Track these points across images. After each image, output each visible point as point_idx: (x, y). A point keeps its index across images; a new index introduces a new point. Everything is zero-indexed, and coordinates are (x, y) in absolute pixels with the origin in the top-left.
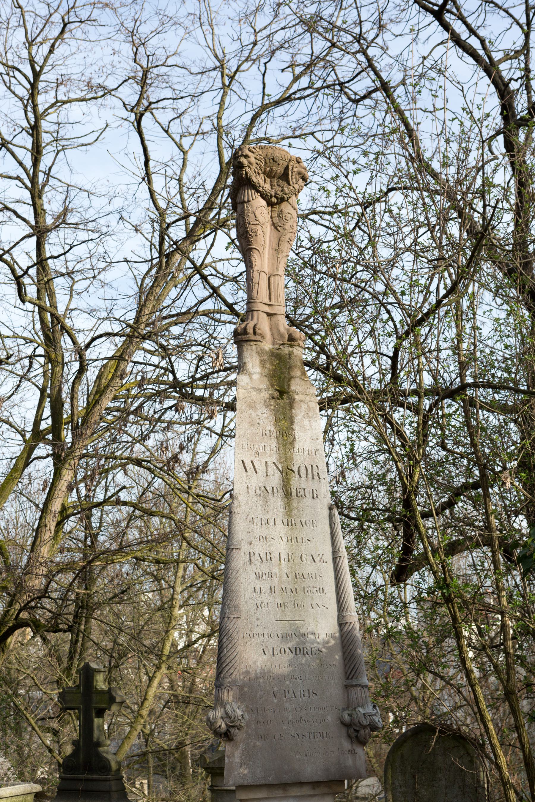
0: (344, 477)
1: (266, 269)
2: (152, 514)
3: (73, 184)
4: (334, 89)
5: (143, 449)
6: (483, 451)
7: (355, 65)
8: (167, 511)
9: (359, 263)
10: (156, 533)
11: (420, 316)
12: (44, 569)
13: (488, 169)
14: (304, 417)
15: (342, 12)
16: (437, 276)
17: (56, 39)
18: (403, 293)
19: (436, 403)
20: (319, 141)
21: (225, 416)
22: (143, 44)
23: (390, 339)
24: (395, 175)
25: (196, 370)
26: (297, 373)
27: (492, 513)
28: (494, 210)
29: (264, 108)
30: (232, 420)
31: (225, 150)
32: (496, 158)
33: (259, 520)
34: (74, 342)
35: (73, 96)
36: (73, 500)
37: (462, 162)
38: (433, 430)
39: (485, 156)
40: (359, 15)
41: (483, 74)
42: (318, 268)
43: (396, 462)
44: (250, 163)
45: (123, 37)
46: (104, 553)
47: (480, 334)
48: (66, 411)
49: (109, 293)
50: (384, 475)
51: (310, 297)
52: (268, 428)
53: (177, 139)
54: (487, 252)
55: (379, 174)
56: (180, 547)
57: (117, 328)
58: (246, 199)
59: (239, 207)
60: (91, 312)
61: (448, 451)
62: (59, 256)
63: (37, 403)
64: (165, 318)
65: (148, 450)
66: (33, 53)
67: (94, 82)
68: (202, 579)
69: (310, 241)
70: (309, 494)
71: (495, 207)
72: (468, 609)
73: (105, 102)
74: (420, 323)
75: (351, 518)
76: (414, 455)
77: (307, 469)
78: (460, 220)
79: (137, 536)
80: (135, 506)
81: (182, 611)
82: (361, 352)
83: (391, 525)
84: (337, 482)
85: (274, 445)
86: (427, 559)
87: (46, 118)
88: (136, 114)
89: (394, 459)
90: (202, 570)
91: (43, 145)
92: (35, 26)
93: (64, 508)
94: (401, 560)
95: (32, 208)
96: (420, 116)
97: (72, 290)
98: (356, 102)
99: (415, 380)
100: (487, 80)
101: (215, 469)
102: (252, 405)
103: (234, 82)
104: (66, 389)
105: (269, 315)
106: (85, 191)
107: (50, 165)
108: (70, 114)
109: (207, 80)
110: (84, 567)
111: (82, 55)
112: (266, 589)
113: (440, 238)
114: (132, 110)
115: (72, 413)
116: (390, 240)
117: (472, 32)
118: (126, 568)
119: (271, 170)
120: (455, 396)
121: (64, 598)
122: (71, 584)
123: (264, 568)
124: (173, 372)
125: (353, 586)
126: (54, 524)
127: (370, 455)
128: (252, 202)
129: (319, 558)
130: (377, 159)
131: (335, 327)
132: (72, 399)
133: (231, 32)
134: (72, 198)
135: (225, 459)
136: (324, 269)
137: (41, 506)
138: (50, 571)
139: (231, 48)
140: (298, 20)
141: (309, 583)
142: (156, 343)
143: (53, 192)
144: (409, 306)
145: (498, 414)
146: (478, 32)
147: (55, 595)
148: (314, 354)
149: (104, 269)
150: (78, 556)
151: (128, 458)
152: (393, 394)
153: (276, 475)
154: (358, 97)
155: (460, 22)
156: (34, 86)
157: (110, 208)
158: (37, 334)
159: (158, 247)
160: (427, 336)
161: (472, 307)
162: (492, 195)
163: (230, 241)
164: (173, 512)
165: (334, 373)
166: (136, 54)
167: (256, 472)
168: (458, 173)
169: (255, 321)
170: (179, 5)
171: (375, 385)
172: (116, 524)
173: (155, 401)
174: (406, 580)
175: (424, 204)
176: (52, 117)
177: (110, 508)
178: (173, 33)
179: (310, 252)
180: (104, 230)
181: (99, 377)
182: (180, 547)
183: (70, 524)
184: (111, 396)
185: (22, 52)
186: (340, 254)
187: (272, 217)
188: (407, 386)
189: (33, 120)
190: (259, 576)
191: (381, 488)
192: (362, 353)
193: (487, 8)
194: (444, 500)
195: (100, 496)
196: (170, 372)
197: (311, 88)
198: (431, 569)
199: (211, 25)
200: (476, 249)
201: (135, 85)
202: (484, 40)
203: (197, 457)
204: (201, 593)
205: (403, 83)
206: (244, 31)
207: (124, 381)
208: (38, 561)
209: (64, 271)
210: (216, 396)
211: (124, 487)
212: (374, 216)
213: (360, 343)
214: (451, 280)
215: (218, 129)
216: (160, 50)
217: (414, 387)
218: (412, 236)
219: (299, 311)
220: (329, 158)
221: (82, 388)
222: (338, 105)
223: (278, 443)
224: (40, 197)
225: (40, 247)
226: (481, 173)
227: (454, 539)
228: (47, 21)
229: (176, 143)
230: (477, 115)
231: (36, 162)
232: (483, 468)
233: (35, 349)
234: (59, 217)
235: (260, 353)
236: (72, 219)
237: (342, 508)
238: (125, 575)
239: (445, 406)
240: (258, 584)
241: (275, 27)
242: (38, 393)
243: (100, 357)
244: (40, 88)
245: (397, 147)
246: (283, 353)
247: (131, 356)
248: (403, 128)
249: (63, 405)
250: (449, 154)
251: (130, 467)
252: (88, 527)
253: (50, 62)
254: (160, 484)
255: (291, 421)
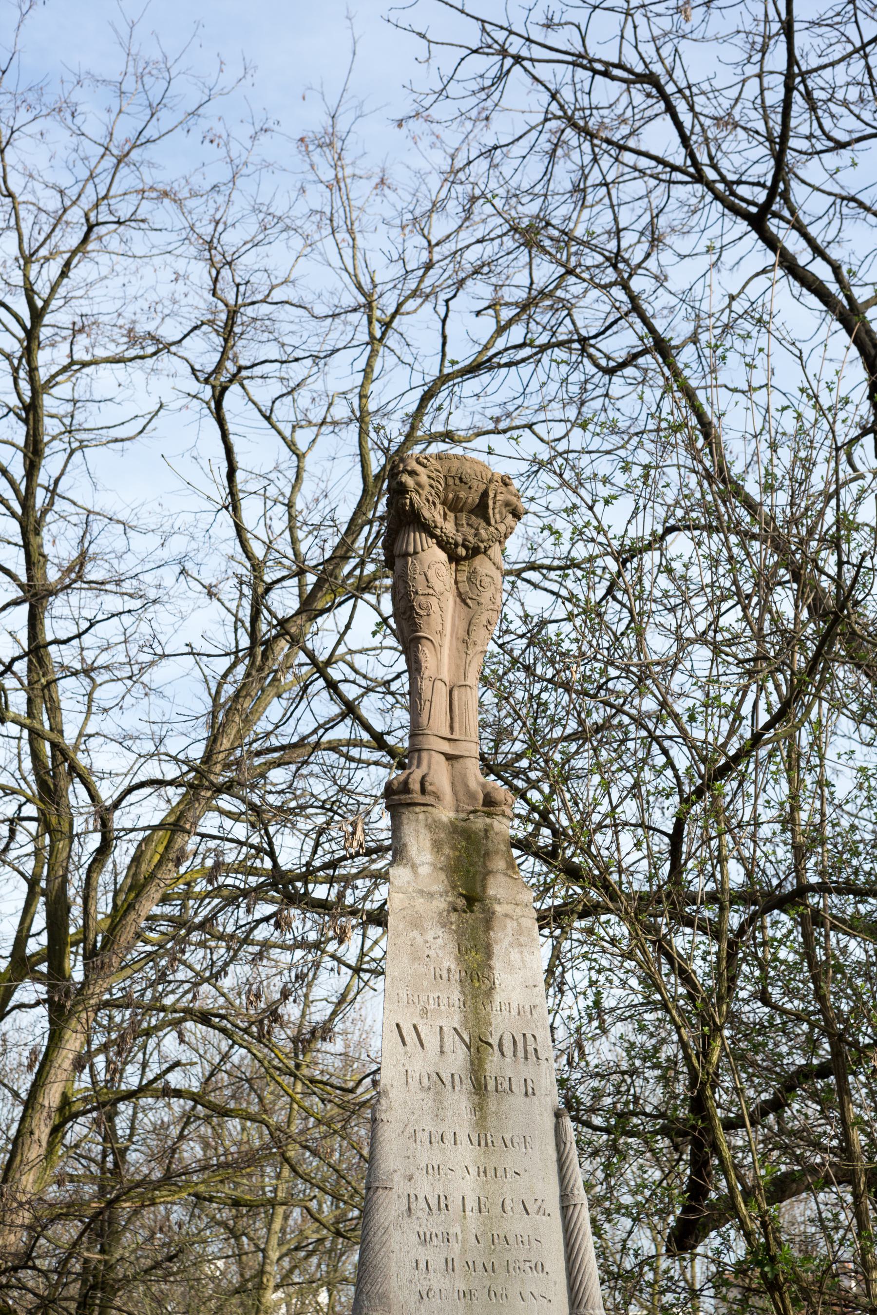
0: (582, 1055)
1: (445, 675)
2: (226, 1113)
3: (97, 510)
4: (570, 349)
5: (213, 991)
6: (838, 1008)
7: (607, 308)
8: (254, 1109)
9: (612, 664)
10: (233, 1149)
11: (723, 761)
12: (26, 1214)
13: (847, 496)
14: (511, 945)
15: (586, 213)
16: (754, 687)
17: (74, 253)
18: (692, 719)
19: (751, 920)
20: (542, 440)
21: (364, 936)
22: (229, 264)
23: (667, 803)
24: (677, 502)
25: (315, 852)
26: (499, 864)
27: (854, 1124)
28: (858, 572)
29: (443, 379)
30: (376, 943)
31: (372, 453)
32: (862, 477)
33: (427, 1134)
34: (94, 796)
35: (100, 353)
36: (83, 1085)
37: (799, 484)
38: (745, 968)
39: (841, 475)
40: (616, 219)
41: (837, 325)
42: (539, 670)
43: (678, 1028)
44: (419, 484)
45: (193, 251)
46: (138, 1184)
47: (832, 793)
48: (75, 920)
49: (157, 708)
50: (656, 1049)
51: (524, 724)
52: (446, 964)
53: (287, 433)
54: (845, 645)
55: (650, 504)
56: (278, 1177)
57: (172, 771)
58: (411, 550)
59: (398, 563)
60: (124, 740)
61: (775, 1007)
62: (70, 639)
63: (22, 904)
64: (258, 754)
65: (223, 995)
66: (32, 276)
67: (142, 328)
68: (315, 1237)
69: (525, 623)
70: (518, 1088)
71: (860, 566)
72: (811, 1304)
73: (160, 365)
74: (722, 772)
75: (596, 1128)
76: (712, 1016)
77: (515, 1042)
78: (795, 586)
79: (199, 1153)
80: (196, 1098)
81: (280, 1294)
82: (616, 825)
83: (667, 1141)
84: (569, 1063)
85: (456, 995)
86: (734, 1208)
87: (52, 391)
88: (213, 387)
89: (673, 1021)
90: (317, 1220)
91: (46, 439)
92: (37, 227)
93: (65, 1101)
94: (686, 1210)
95: (22, 553)
96: (724, 399)
97: (90, 700)
98: (610, 372)
99: (713, 875)
100: (844, 338)
101: (345, 1033)
102: (416, 923)
103: (390, 332)
104: (76, 881)
105: (450, 758)
106: (118, 522)
107: (57, 474)
108: (95, 385)
109: (341, 327)
110: (100, 1213)
111: (121, 280)
112: (438, 1263)
113: (761, 619)
114: (206, 381)
115: (86, 926)
116: (669, 620)
117: (818, 251)
118: (178, 1213)
119: (457, 498)
120: (786, 906)
121: (62, 1269)
122: (75, 1244)
123: (434, 1225)
124: (272, 855)
125: (598, 1257)
126: (47, 1131)
127: (631, 1014)
128: (422, 555)
129: (536, 1207)
130: (646, 476)
131: (567, 779)
132: (86, 900)
133: (387, 246)
134: (95, 534)
135: (363, 1012)
136: (550, 673)
137: (24, 1096)
138: (37, 1219)
139: (386, 273)
140: (506, 227)
141: (518, 1253)
142: (243, 800)
143: (62, 524)
144: (704, 742)
145: (864, 940)
146: (828, 251)
147: (43, 1264)
148: (530, 828)
149: (152, 664)
150: (90, 1189)
151: (186, 1010)
152: (673, 903)
153: (459, 1052)
154: (612, 364)
155: (795, 234)
156: (31, 335)
157: (164, 554)
158: (24, 779)
159: (248, 625)
160: (735, 795)
161: (817, 745)
162: (853, 545)
163: (379, 620)
164: (265, 1111)
165: (567, 862)
166: (215, 281)
167: (422, 1045)
168: (792, 504)
169: (424, 768)
170: (294, 195)
171: (640, 885)
172: (160, 1129)
173: (238, 907)
174: (695, 1247)
175: (731, 558)
176: (63, 390)
177: (150, 1100)
178: (284, 243)
179: (525, 641)
180: (152, 594)
181: (137, 860)
182: (278, 1177)
183: (77, 1130)
184: (158, 896)
185: (13, 274)
186: (579, 648)
187: (456, 582)
188: (699, 885)
189: (29, 393)
190: (425, 1240)
191: (649, 1073)
192: (617, 826)
193: (845, 210)
194: (764, 1096)
195: (132, 1078)
196: (266, 853)
197: (531, 345)
198: (742, 1226)
199: (350, 231)
200: (825, 640)
201: (213, 336)
202: (839, 267)
203: (313, 1009)
204: (314, 1260)
205: (694, 339)
206: (409, 245)
207: (182, 870)
208: (15, 1199)
209: (78, 666)
210: (349, 900)
211: (177, 1064)
212: (640, 579)
213: (614, 809)
214: (780, 697)
215: (362, 418)
216: (259, 274)
217: (711, 886)
218: (710, 616)
219: (504, 748)
220: (561, 475)
221: (105, 878)
222: (577, 377)
223: (463, 992)
224: (37, 533)
225: (34, 622)
226: (833, 502)
227: (783, 1168)
228: (59, 220)
229: (284, 438)
230: (826, 400)
231: (32, 469)
232: (837, 1040)
233: (20, 806)
234: (70, 570)
235: (433, 826)
236: (94, 572)
237: (578, 1110)
238: (176, 1228)
239: (768, 924)
240: (422, 1254)
241: (465, 237)
242: (24, 887)
243: (141, 824)
244: (42, 337)
245: (682, 456)
246: (473, 827)
247: (195, 824)
248: (693, 421)
249: (69, 911)
250: (776, 470)
251: (189, 1025)
252: (110, 1136)
253: (62, 291)
254: (242, 1059)
255: (488, 951)
